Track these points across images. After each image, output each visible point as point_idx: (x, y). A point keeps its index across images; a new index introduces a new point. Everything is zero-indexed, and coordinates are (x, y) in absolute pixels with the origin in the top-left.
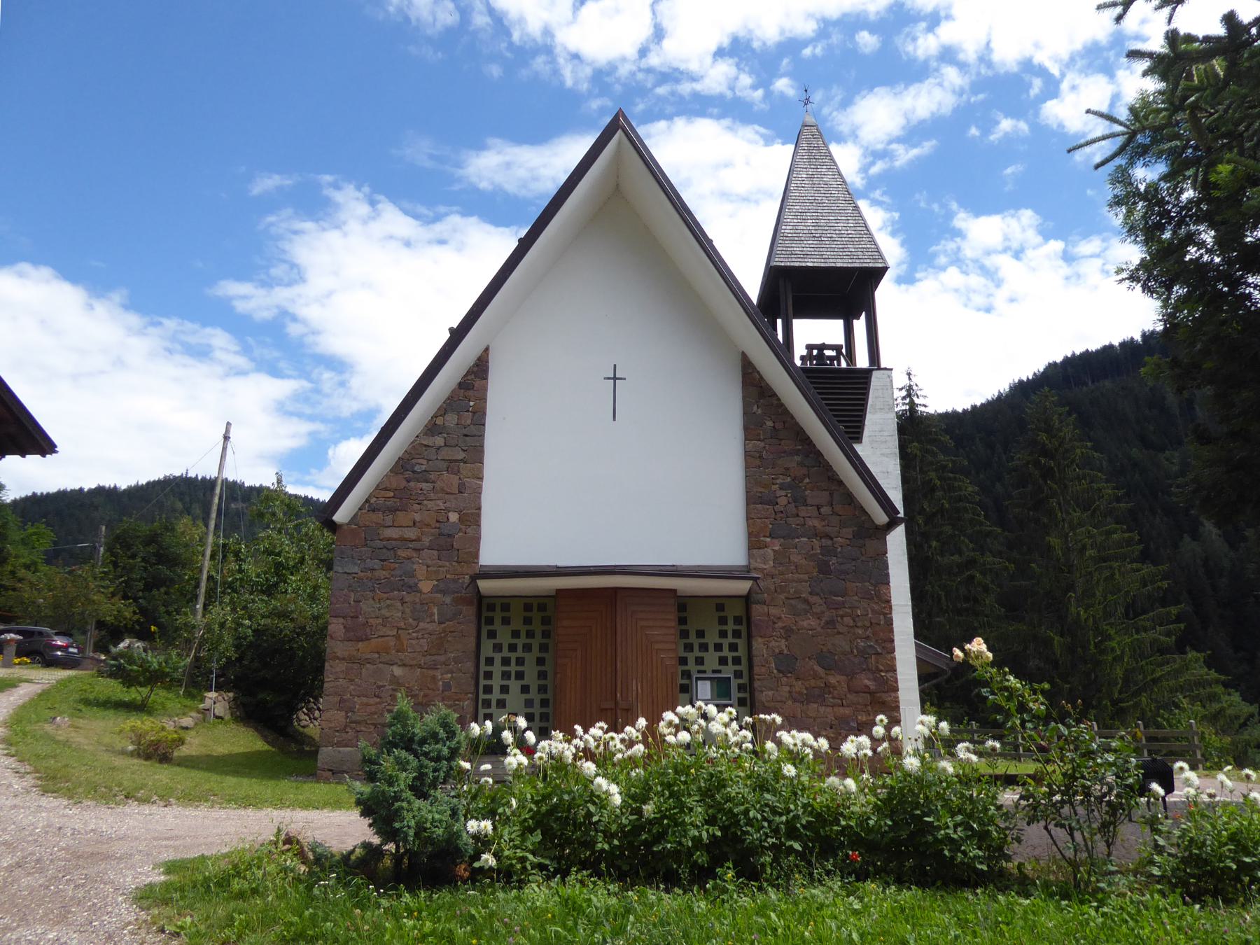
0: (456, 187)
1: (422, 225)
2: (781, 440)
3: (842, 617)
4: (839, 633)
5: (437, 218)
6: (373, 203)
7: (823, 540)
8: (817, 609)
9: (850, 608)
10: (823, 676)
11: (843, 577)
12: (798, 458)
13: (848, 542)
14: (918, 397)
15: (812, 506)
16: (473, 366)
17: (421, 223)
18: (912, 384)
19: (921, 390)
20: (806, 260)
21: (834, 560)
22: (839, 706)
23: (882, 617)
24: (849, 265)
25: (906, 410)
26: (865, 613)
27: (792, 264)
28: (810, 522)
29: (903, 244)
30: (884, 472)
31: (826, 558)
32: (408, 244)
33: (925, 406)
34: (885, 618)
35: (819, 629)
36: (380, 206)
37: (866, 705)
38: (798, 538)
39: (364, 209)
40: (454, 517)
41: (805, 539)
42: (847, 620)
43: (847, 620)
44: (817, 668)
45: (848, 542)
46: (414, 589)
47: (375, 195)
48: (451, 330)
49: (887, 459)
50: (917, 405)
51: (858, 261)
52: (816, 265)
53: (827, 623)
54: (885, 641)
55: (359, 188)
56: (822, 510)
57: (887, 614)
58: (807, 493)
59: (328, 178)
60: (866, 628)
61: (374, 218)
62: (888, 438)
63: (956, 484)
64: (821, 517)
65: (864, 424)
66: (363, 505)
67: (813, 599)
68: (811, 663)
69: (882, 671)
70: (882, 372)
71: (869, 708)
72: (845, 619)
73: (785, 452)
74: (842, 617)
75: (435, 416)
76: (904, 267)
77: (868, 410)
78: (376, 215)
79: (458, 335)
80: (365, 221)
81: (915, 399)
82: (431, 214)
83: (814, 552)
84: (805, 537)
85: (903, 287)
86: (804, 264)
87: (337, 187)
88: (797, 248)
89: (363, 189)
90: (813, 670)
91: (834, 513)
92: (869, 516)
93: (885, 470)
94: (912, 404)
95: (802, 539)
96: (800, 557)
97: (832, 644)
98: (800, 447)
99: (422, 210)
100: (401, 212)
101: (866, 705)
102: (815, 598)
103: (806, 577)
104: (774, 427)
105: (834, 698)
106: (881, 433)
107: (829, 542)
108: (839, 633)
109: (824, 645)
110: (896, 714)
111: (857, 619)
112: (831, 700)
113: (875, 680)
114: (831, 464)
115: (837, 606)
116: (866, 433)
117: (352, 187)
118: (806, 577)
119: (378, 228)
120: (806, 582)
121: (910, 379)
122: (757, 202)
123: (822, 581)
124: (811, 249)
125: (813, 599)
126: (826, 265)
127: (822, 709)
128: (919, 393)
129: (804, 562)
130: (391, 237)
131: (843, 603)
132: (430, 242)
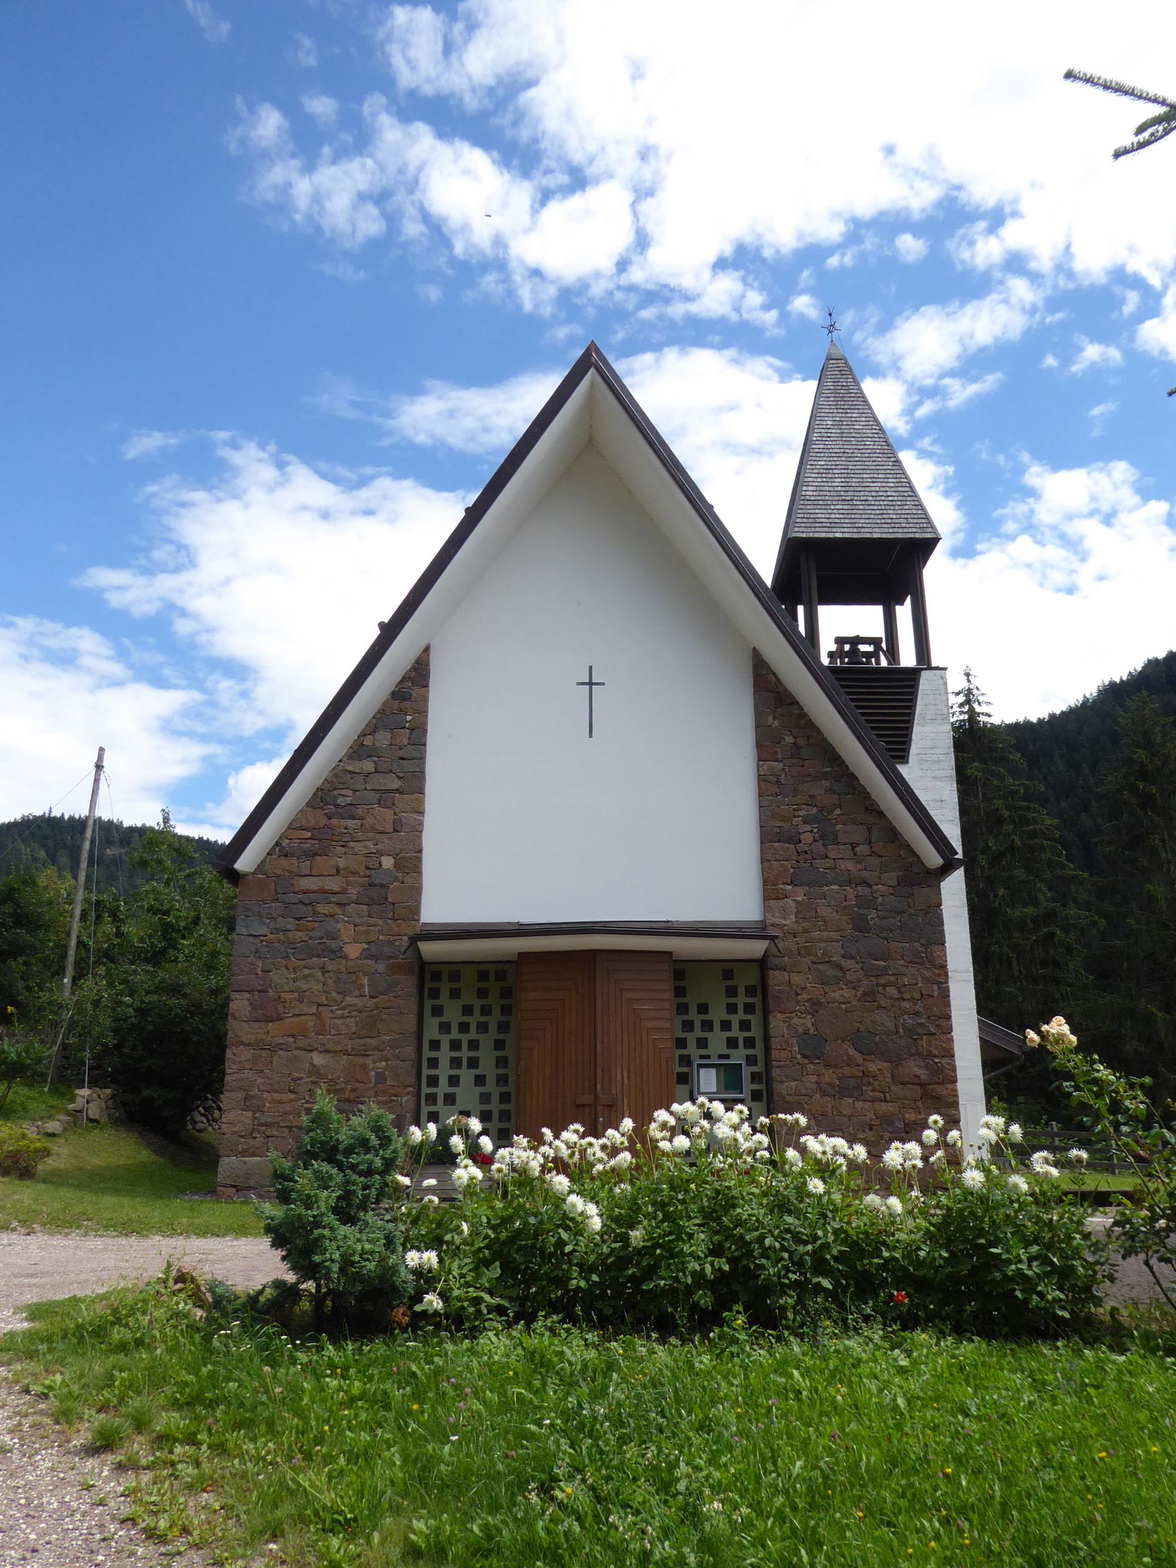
0: (386, 443)
1: (343, 492)
3: (884, 986)
4: (880, 1007)
5: (362, 483)
6: (281, 465)
8: (850, 976)
9: (893, 975)
10: (860, 1062)
11: (884, 935)
14: (979, 704)
16: (410, 671)
21: (873, 913)
23: (935, 987)
28: (842, 865)
29: (958, 507)
32: (325, 515)
33: (989, 716)
34: (939, 988)
35: (854, 1002)
36: (289, 469)
39: (269, 473)
40: (388, 862)
44: (852, 1052)
46: (338, 954)
48: (382, 626)
49: (941, 784)
53: (865, 994)
55: (262, 446)
56: (857, 849)
59: (222, 435)
61: (282, 484)
65: (911, 740)
66: (273, 848)
67: (847, 964)
69: (935, 1056)
71: (920, 1104)
72: (888, 989)
74: (884, 986)
75: (363, 735)
76: (961, 536)
78: (284, 481)
79: (390, 631)
80: (271, 489)
81: (976, 706)
82: (354, 477)
85: (960, 561)
87: (234, 445)
90: (848, 1055)
93: (938, 797)
97: (872, 1022)
99: (344, 472)
100: (316, 476)
103: (837, 935)
105: (874, 1091)
106: (933, 751)
107: (867, 891)
108: (880, 1007)
113: (926, 1067)
117: (253, 445)
118: (837, 935)
119: (286, 497)
121: (969, 681)
122: (770, 454)
125: (847, 964)
127: (859, 1105)
128: (981, 699)
129: (835, 916)
130: (304, 508)
132: (353, 513)
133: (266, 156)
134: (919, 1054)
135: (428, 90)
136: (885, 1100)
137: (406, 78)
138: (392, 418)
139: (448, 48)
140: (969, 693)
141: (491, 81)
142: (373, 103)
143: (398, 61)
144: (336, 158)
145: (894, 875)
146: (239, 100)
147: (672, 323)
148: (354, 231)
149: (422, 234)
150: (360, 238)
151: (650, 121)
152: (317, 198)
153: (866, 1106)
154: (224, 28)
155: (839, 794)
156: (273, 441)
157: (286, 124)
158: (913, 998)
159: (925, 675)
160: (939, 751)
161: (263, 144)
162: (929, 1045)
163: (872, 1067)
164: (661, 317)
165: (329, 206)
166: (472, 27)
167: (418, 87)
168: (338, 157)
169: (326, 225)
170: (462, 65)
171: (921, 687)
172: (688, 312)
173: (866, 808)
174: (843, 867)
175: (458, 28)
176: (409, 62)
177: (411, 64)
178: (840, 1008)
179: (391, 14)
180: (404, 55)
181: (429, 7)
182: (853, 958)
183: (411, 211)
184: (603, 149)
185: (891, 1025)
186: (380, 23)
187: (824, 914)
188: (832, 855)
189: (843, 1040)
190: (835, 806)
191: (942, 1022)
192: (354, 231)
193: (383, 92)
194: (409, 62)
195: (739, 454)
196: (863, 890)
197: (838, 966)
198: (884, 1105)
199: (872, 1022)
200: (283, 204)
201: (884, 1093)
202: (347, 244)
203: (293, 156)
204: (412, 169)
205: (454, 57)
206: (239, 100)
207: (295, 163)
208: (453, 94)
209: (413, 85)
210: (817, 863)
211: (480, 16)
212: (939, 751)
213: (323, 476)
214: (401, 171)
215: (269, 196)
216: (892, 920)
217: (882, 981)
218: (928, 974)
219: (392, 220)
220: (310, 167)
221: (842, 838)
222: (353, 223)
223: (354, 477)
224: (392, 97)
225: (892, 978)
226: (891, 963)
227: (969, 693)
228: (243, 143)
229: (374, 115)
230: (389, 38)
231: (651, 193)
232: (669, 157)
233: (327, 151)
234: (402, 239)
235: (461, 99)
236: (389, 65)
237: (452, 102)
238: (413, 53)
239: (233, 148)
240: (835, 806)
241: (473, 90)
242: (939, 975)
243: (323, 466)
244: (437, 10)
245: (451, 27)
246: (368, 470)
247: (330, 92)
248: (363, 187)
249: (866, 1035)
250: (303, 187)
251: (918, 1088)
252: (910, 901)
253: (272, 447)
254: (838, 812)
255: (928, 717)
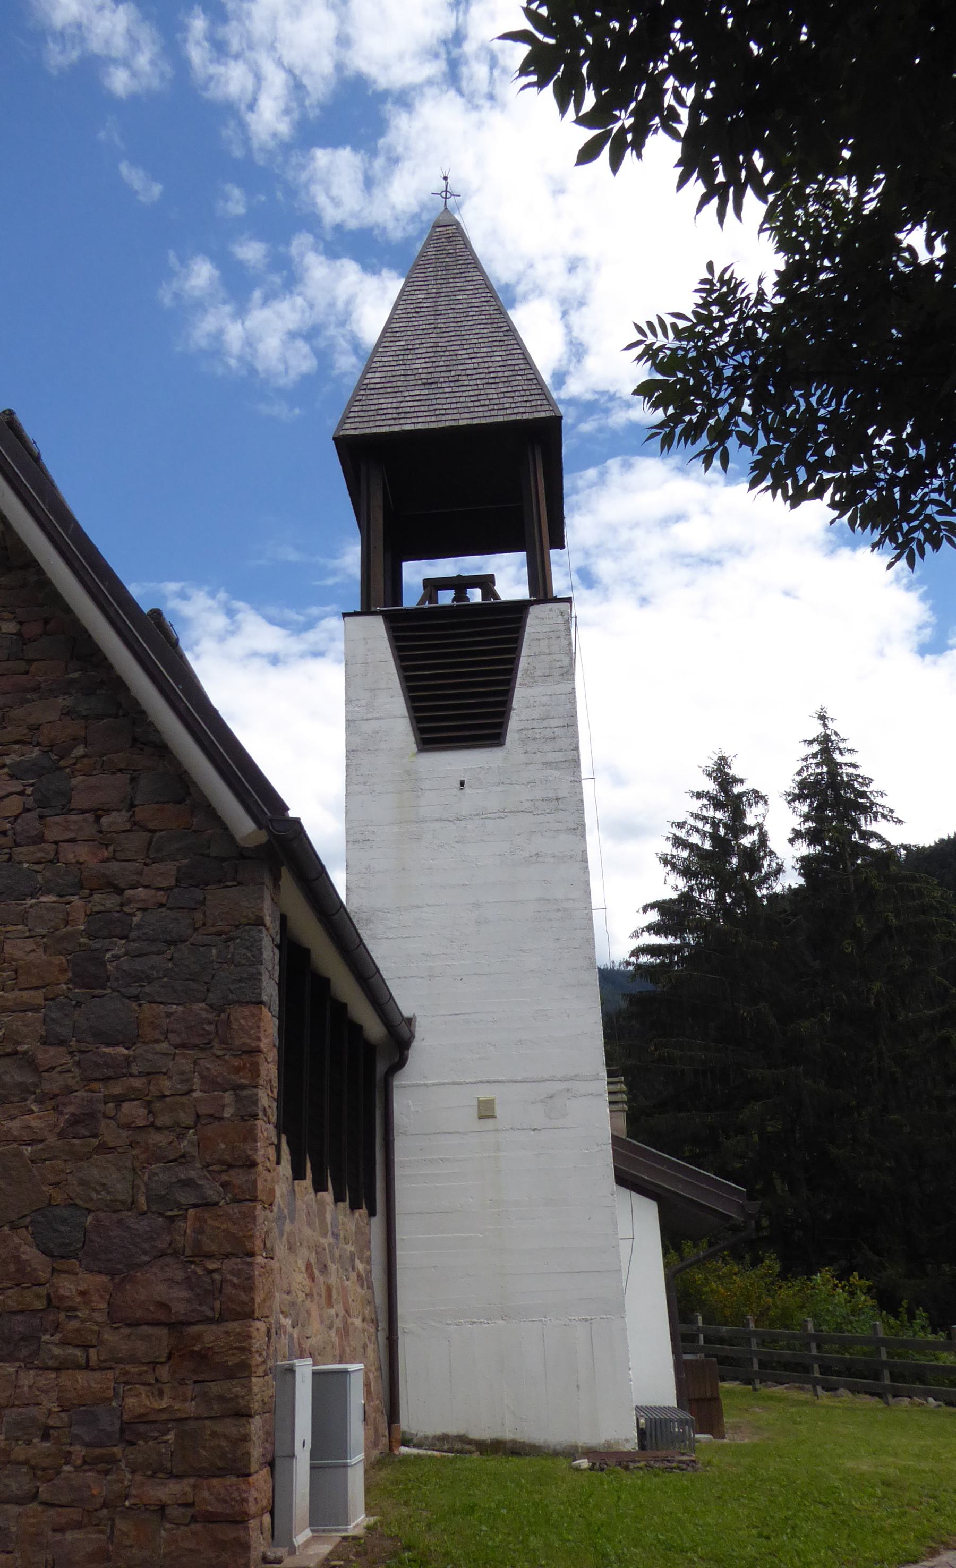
0: (330, 581)
1: (291, 635)
2: (30, 661)
3: (119, 1100)
4: (104, 1148)
5: (310, 625)
6: (231, 613)
7: (96, 897)
8: (53, 1083)
9: (140, 1075)
10: (44, 1275)
11: (134, 991)
12: (63, 702)
13: (161, 897)
14: (841, 753)
15: (84, 812)
17: (289, 632)
18: (829, 732)
19: (843, 740)
20: (402, 421)
21: (119, 948)
22: (79, 1367)
23: (228, 1097)
24: (484, 421)
25: (821, 774)
26: (184, 1087)
27: (375, 430)
28: (70, 854)
29: (924, 598)
30: (549, 800)
31: (96, 945)
32: (275, 660)
33: (855, 766)
34: (238, 1099)
35: (52, 1140)
36: (239, 616)
37: (154, 1364)
38: (32, 896)
39: (220, 622)
41: (51, 898)
42: (133, 1111)
43: (133, 1111)
44: (30, 1253)
45: (161, 897)
47: (234, 602)
49: (557, 773)
50: (840, 765)
51: (501, 412)
52: (420, 426)
53: (75, 1121)
54: (231, 1166)
55: (212, 595)
56: (104, 820)
57: (243, 1087)
58: (74, 782)
59: (173, 587)
60: (180, 1131)
61: (233, 633)
62: (559, 732)
63: (914, 886)
64: (103, 839)
65: (511, 709)
67: (47, 1055)
68: (17, 1240)
69: (210, 1256)
70: (549, 606)
71: (164, 1372)
72: (126, 1106)
73: (37, 689)
74: (119, 1100)
76: (928, 631)
77: (519, 680)
78: (234, 630)
80: (222, 638)
81: (837, 756)
82: (301, 619)
83: (69, 928)
84: (48, 892)
85: (928, 658)
86: (396, 429)
87: (183, 596)
88: (387, 404)
89: (218, 596)
90: (17, 1259)
91: (136, 825)
92: (226, 829)
93: (551, 794)
94: (834, 766)
95: (43, 899)
96: (30, 945)
97: (82, 1183)
98: (76, 675)
99: (292, 615)
100: (264, 621)
101: (154, 1364)
102: (52, 1051)
103: (36, 997)
104: (19, 634)
105: (64, 1343)
106: (545, 723)
107: (112, 901)
108: (104, 1148)
109: (57, 1184)
110: (238, 1390)
111: (157, 1105)
112: (57, 1351)
113: (188, 1282)
114: (145, 706)
115: (110, 1073)
116: (514, 723)
117: (202, 593)
118: (36, 997)
119: (237, 645)
120: (36, 1009)
121: (825, 725)
122: (719, 563)
123: (78, 1005)
124: (415, 404)
125: (47, 1055)
126: (440, 425)
127: (27, 1379)
128: (841, 745)
129: (39, 956)
130: (255, 654)
131: (128, 1061)
132: (302, 655)
133: (199, 306)
134: (176, 1254)
135: (353, 224)
136: (87, 1367)
137: (331, 215)
138: (337, 558)
139: (369, 183)
140: (825, 740)
141: (415, 209)
142: (301, 245)
143: (322, 199)
144: (267, 300)
145: (170, 867)
146: (172, 254)
147: (614, 434)
148: (287, 370)
149: (354, 366)
150: (293, 374)
151: (577, 233)
152: (250, 342)
153: (42, 1382)
154: (157, 189)
155: (85, 718)
156: (222, 589)
157: (217, 273)
158: (177, 1124)
159: (536, 615)
160: (554, 723)
161: (197, 293)
162: (200, 1231)
163: (67, 1287)
164: (601, 430)
165: (262, 348)
166: (394, 161)
167: (343, 221)
168: (269, 298)
169: (260, 367)
170: (386, 196)
171: (528, 629)
172: (629, 420)
173: (135, 740)
174: (70, 857)
175: (379, 162)
176: (332, 199)
177: (336, 202)
178: (19, 1154)
179: (313, 159)
180: (327, 194)
181: (348, 149)
182: (62, 1043)
183: (344, 344)
184: (531, 266)
185: (121, 1190)
186: (303, 167)
187: (18, 954)
188: (53, 834)
189: (14, 1227)
190: (76, 740)
191: (237, 1177)
192: (287, 370)
193: (310, 231)
194: (332, 199)
195: (688, 565)
196: (105, 901)
197: (29, 1062)
198: (82, 1378)
199: (82, 1183)
200: (217, 350)
201: (86, 1347)
202: (282, 381)
203: (225, 302)
204: (340, 305)
205: (376, 191)
206: (172, 254)
207: (228, 309)
208: (377, 225)
209: (338, 219)
210: (22, 852)
211: (400, 149)
212: (554, 723)
213: (272, 621)
214: (332, 305)
215: (203, 343)
216: (156, 959)
217: (117, 1089)
218: (215, 1069)
219: (324, 356)
220: (241, 312)
221: (79, 801)
222: (285, 362)
223: (301, 619)
224: (318, 237)
225: (137, 1083)
226: (140, 1049)
227: (825, 740)
228: (177, 296)
229: (302, 255)
230: (311, 180)
231: (582, 303)
232: (598, 268)
233: (257, 295)
234: (336, 372)
235: (384, 229)
236: (315, 204)
237: (376, 232)
238: (335, 191)
239: (167, 300)
240: (76, 740)
241: (397, 220)
242: (238, 1070)
243: (273, 611)
244: (355, 149)
245: (370, 163)
246: (314, 611)
247: (260, 236)
248: (292, 326)
249: (65, 1213)
250: (234, 333)
251: (163, 1331)
252: (198, 915)
253: (222, 596)
254: (80, 751)
255: (539, 673)
